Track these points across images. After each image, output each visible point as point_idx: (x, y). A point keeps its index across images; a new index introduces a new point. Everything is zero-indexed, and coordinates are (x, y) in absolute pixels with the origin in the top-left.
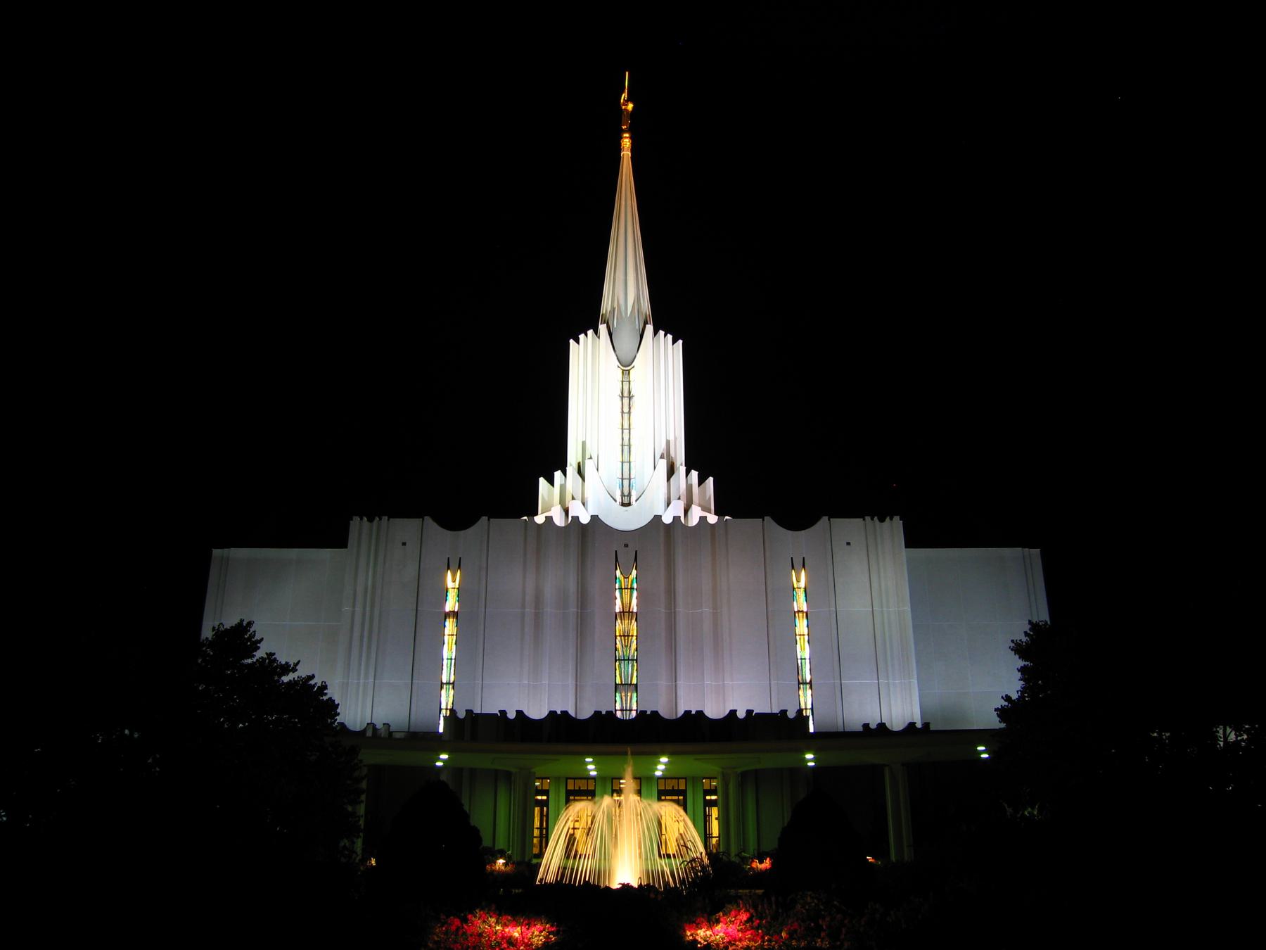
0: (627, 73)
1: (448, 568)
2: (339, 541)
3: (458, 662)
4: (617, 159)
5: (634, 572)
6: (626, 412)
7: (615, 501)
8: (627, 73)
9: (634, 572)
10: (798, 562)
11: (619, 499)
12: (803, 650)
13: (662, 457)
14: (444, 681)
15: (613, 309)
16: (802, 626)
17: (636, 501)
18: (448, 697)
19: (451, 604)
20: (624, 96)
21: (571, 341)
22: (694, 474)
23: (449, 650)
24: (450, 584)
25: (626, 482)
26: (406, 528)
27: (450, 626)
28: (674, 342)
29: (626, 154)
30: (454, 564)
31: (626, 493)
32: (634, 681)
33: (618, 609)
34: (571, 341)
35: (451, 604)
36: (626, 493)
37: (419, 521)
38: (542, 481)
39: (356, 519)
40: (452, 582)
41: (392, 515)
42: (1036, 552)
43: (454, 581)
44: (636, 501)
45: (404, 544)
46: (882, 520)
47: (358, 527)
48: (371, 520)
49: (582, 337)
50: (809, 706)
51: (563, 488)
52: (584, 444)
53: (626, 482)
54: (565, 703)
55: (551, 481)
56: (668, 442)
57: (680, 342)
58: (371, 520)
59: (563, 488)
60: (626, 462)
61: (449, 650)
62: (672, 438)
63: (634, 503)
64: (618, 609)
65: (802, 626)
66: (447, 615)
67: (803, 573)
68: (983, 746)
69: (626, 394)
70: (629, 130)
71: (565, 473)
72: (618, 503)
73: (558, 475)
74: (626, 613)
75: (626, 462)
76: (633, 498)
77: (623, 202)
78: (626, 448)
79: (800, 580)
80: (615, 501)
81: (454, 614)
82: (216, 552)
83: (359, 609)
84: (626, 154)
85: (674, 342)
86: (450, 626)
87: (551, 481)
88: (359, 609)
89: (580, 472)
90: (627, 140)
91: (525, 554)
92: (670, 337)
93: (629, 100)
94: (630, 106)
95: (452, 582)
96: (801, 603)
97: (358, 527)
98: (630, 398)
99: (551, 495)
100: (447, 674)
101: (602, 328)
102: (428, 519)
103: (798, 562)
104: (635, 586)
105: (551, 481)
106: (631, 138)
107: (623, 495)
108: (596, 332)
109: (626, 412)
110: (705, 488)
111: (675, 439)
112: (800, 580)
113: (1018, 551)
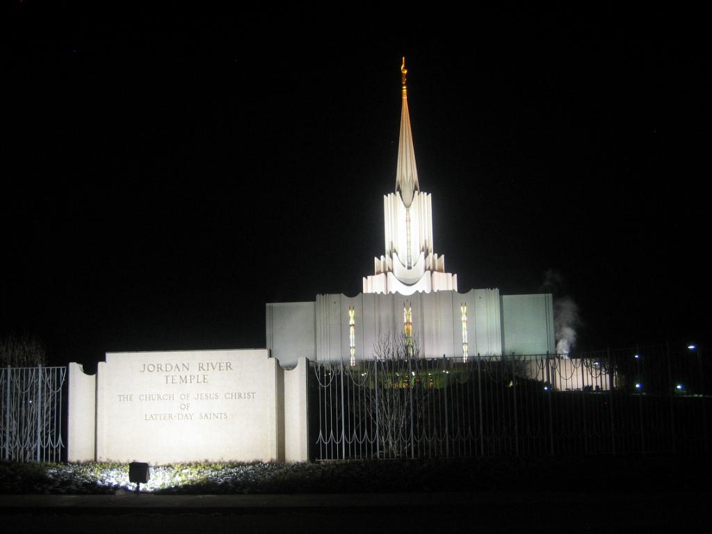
2: (314, 299)
3: (356, 340)
4: (401, 100)
6: (408, 228)
7: (404, 266)
9: (410, 309)
11: (406, 265)
12: (465, 333)
15: (402, 180)
16: (464, 325)
19: (352, 322)
20: (403, 66)
22: (436, 255)
23: (352, 337)
24: (350, 315)
27: (352, 329)
28: (427, 194)
29: (405, 98)
33: (405, 321)
35: (352, 322)
39: (318, 295)
40: (351, 314)
41: (330, 293)
42: (550, 295)
48: (323, 295)
49: (389, 195)
51: (384, 263)
58: (323, 295)
59: (384, 263)
61: (352, 337)
63: (413, 267)
66: (351, 326)
68: (692, 345)
70: (406, 84)
73: (382, 257)
74: (408, 323)
79: (464, 310)
80: (404, 266)
81: (353, 325)
82: (267, 305)
83: (322, 326)
84: (405, 98)
85: (427, 194)
86: (352, 329)
88: (322, 326)
89: (391, 257)
91: (375, 307)
92: (426, 193)
94: (406, 72)
95: (351, 314)
98: (410, 221)
100: (352, 344)
102: (342, 294)
105: (380, 259)
106: (406, 89)
109: (408, 228)
113: (543, 295)
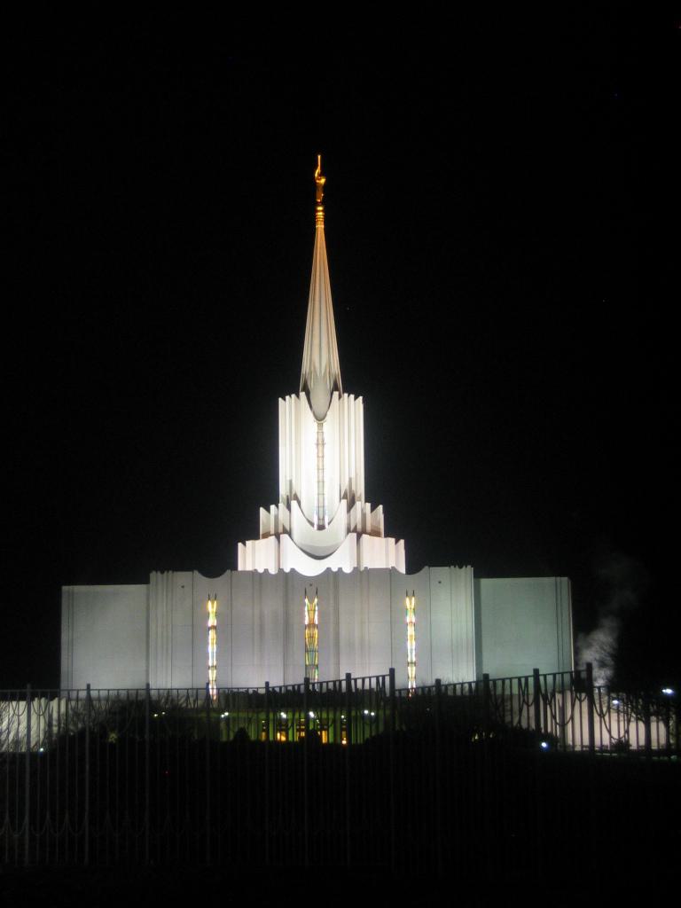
0: (319, 157)
1: (209, 599)
2: (146, 581)
5: (316, 600)
6: (321, 457)
7: (312, 524)
8: (319, 157)
9: (316, 600)
10: (410, 592)
11: (316, 521)
13: (344, 498)
14: (210, 664)
16: (411, 631)
17: (329, 524)
18: (213, 673)
19: (212, 621)
20: (318, 171)
21: (280, 399)
23: (212, 648)
25: (321, 509)
26: (182, 578)
28: (356, 398)
29: (320, 226)
30: (212, 597)
31: (321, 517)
32: (414, 660)
33: (307, 622)
34: (280, 399)
35: (212, 621)
36: (321, 517)
37: (191, 573)
38: (262, 510)
40: (212, 607)
43: (213, 607)
44: (329, 524)
45: (183, 587)
46: (461, 567)
47: (154, 576)
49: (287, 397)
50: (414, 676)
51: (276, 518)
52: (291, 482)
53: (321, 509)
54: (277, 681)
55: (268, 510)
56: (350, 480)
57: (361, 398)
60: (321, 494)
61: (212, 648)
62: (353, 476)
63: (327, 526)
64: (307, 622)
65: (411, 631)
66: (209, 629)
67: (413, 599)
69: (320, 442)
70: (323, 203)
71: (277, 506)
72: (316, 526)
73: (273, 507)
75: (321, 494)
76: (327, 521)
77: (318, 274)
78: (321, 484)
79: (410, 603)
82: (65, 588)
84: (320, 226)
85: (356, 398)
87: (268, 510)
90: (321, 213)
92: (352, 396)
93: (321, 175)
94: (323, 181)
95: (212, 607)
96: (410, 618)
97: (154, 576)
99: (268, 520)
100: (212, 661)
101: (302, 394)
102: (196, 573)
103: (410, 592)
104: (317, 608)
107: (319, 519)
108: (298, 396)
109: (321, 457)
110: (376, 515)
111: (356, 475)
112: (410, 603)
